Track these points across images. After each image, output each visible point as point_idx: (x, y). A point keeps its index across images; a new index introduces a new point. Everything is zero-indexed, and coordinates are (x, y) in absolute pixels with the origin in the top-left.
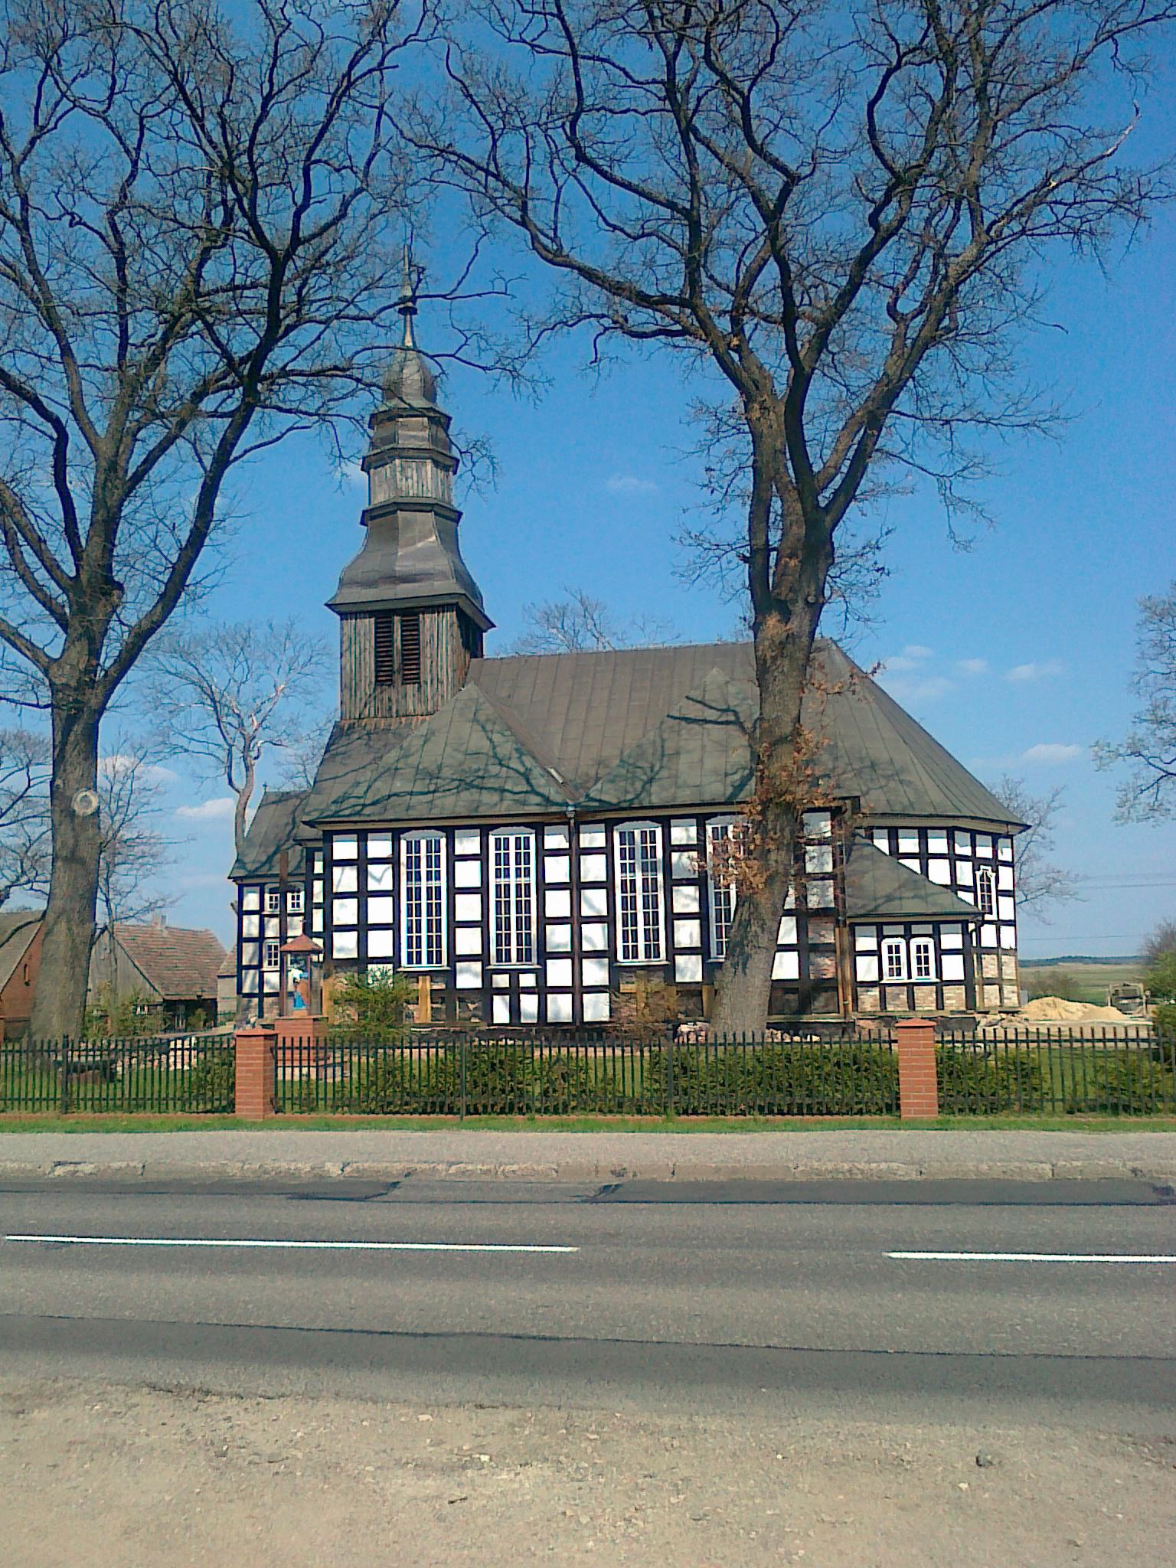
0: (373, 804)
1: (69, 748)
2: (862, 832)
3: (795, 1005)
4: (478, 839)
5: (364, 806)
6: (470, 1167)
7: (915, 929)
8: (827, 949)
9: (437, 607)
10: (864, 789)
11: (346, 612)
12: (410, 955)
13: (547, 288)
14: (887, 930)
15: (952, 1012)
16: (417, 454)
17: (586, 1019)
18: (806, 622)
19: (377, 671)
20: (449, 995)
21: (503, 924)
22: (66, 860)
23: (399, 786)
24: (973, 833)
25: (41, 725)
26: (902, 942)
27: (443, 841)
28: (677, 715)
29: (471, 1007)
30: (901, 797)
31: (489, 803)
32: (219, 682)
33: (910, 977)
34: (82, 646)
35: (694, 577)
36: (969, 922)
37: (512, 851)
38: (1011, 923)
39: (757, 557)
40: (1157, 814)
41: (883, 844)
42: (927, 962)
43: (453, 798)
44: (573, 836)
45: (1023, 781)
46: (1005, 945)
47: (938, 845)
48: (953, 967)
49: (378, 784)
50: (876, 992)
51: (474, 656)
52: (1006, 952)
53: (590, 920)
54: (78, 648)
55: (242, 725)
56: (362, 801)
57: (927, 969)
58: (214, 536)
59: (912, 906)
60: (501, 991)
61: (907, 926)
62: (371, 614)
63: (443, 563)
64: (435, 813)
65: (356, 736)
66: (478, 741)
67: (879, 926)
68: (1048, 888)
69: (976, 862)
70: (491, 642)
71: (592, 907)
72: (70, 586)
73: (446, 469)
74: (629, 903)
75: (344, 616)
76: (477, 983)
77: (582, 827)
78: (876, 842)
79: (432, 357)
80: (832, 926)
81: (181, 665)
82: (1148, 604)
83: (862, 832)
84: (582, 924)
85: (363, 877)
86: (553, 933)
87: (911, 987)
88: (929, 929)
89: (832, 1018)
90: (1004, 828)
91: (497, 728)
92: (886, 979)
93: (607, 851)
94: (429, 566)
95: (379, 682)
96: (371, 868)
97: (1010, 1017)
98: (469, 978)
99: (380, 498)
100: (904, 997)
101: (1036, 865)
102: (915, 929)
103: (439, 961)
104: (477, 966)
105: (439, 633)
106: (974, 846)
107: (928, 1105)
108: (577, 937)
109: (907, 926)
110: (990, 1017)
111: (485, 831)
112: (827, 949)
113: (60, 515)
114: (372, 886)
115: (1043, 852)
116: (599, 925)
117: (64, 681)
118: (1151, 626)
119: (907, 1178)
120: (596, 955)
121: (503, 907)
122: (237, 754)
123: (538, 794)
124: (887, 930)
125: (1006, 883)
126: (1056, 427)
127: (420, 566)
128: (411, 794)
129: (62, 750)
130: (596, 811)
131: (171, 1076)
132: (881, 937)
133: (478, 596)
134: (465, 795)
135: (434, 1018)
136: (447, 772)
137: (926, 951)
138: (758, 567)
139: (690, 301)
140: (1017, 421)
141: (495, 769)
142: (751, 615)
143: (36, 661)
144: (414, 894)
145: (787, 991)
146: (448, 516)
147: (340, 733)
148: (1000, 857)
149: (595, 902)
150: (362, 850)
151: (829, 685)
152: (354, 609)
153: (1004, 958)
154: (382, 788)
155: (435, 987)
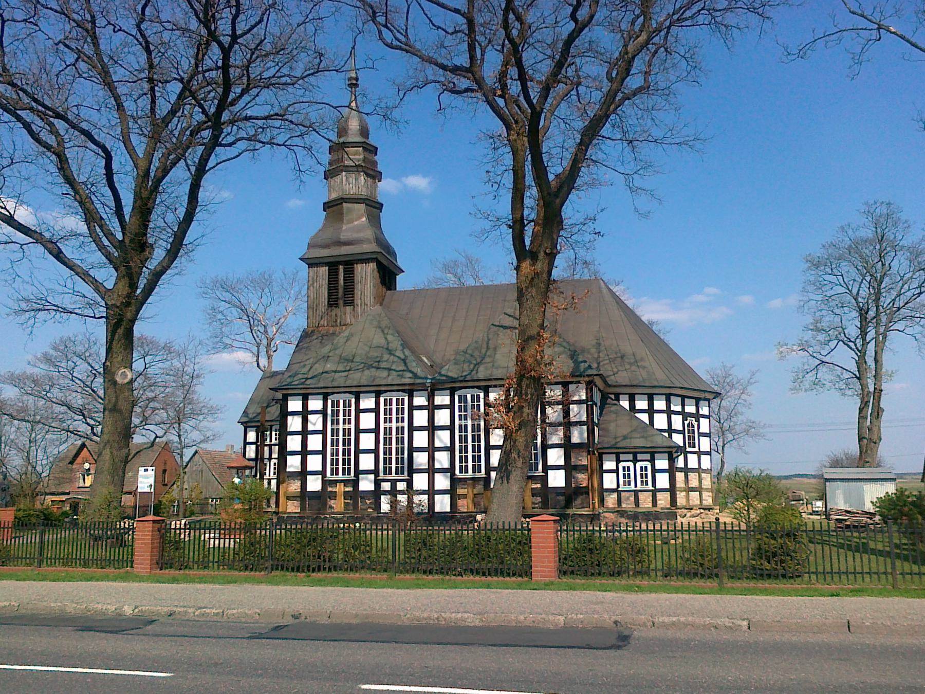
0: (312, 378)
1: (114, 343)
2: (612, 396)
3: (563, 503)
4: (374, 399)
5: (307, 379)
6: (208, 611)
7: (639, 457)
8: (583, 469)
9: (365, 259)
10: (615, 370)
11: (312, 263)
12: (332, 469)
13: (400, 66)
14: (622, 457)
15: (662, 508)
16: (357, 168)
17: (436, 510)
18: (546, 265)
19: (329, 298)
20: (355, 495)
21: (388, 451)
22: (111, 411)
23: (329, 366)
24: (683, 398)
25: (99, 330)
26: (631, 465)
27: (353, 401)
28: (497, 324)
29: (368, 502)
30: (641, 376)
31: (382, 377)
32: (252, 308)
33: (636, 486)
34: (125, 282)
35: (483, 238)
36: (672, 453)
37: (394, 407)
38: (709, 453)
39: (517, 226)
40: (818, 387)
41: (625, 404)
42: (646, 477)
43: (359, 374)
44: (431, 398)
45: (733, 366)
46: (704, 466)
47: (660, 404)
48: (663, 481)
49: (317, 365)
50: (615, 495)
51: (389, 289)
52: (705, 471)
53: (441, 449)
54: (123, 283)
55: (266, 332)
56: (306, 376)
57: (647, 482)
58: (199, 215)
59: (638, 442)
60: (385, 493)
61: (635, 455)
62: (326, 264)
63: (369, 234)
64: (348, 383)
65: (315, 337)
66: (379, 340)
67: (617, 455)
68: (747, 432)
69: (685, 415)
70: (402, 282)
71: (441, 440)
72: (120, 245)
73: (373, 178)
74: (463, 439)
75: (310, 265)
76: (371, 487)
77: (436, 392)
78: (621, 403)
79: (335, 108)
80: (585, 454)
81: (228, 296)
82: (809, 258)
83: (612, 396)
84: (429, 451)
85: (305, 421)
86: (559, 457)
87: (636, 493)
88: (648, 457)
89: (584, 512)
90: (703, 394)
91: (391, 332)
92: (639, 487)
93: (451, 407)
94: (361, 235)
95: (330, 305)
96: (310, 417)
97: (707, 512)
98: (366, 484)
99: (334, 196)
100: (632, 499)
101: (741, 418)
102: (639, 457)
103: (349, 474)
104: (372, 477)
105: (366, 274)
106: (683, 406)
107: (549, 572)
108: (431, 459)
109: (635, 455)
110: (693, 512)
111: (378, 395)
112: (583, 469)
113: (112, 204)
114: (310, 427)
115: (744, 410)
116: (445, 453)
117: (113, 302)
118: (813, 272)
119: (473, 624)
120: (442, 471)
121: (388, 441)
122: (263, 350)
123: (411, 372)
124: (622, 457)
125: (705, 428)
126: (698, 145)
127: (356, 236)
128: (335, 372)
129: (111, 343)
130: (444, 382)
131: (202, 543)
132: (618, 461)
133: (394, 254)
134: (367, 372)
135: (346, 509)
136: (357, 359)
137: (646, 470)
138: (517, 231)
139: (471, 70)
140: (673, 141)
141: (386, 357)
142: (515, 262)
143: (97, 290)
144: (335, 432)
145: (558, 494)
146: (374, 206)
147: (306, 335)
148: (701, 412)
149: (443, 438)
150: (305, 405)
151: (559, 304)
152: (316, 261)
153: (703, 475)
154: (318, 368)
155: (347, 489)
